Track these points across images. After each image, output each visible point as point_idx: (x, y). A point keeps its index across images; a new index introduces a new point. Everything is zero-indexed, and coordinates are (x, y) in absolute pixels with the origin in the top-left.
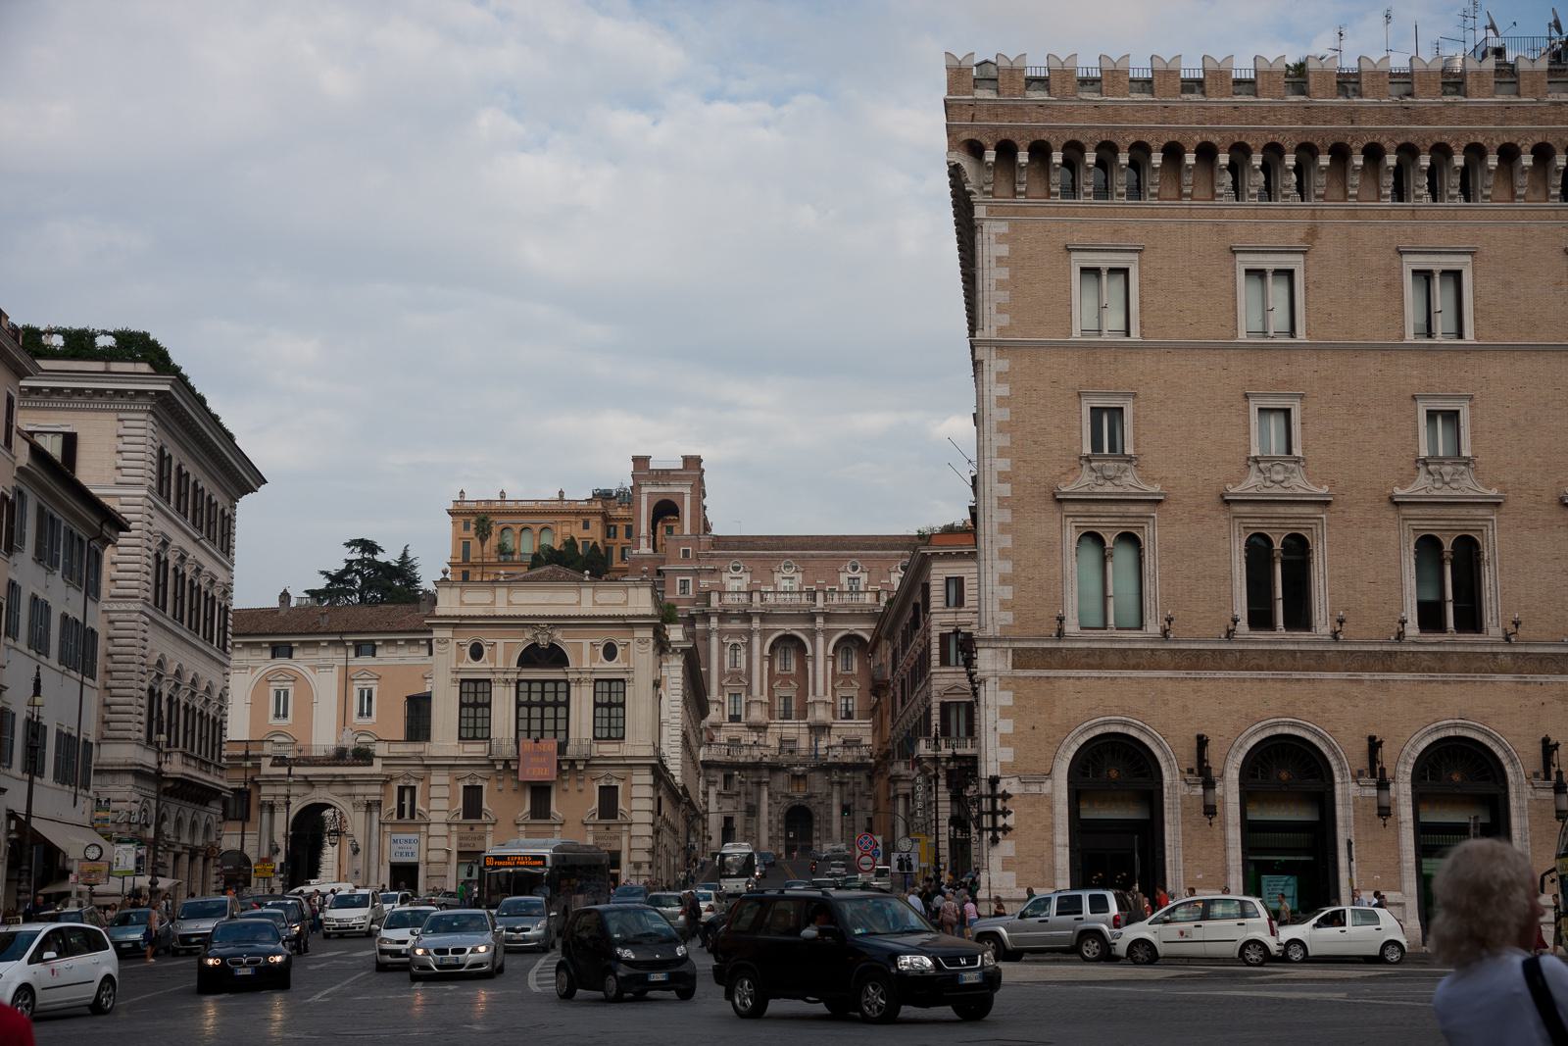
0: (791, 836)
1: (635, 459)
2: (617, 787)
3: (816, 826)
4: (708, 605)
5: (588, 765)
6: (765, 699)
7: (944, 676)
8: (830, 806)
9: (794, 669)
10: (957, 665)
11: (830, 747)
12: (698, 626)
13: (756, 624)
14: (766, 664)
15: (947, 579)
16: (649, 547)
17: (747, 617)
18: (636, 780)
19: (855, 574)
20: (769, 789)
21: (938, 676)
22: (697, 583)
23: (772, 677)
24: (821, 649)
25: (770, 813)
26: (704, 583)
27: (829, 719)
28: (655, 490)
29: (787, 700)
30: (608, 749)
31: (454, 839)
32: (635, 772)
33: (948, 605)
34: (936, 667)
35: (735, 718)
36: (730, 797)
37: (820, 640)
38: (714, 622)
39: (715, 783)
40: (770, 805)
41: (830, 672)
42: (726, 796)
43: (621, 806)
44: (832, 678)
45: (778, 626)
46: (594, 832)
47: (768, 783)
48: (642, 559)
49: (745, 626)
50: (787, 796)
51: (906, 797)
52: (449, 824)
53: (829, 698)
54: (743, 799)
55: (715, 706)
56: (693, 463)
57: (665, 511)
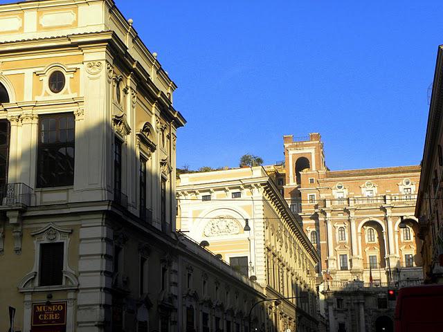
2: (63, 243)
4: (325, 207)
16: (294, 182)
19: (408, 186)
20: (364, 307)
23: (364, 245)
25: (366, 321)
26: (323, 196)
29: (372, 258)
30: (54, 196)
36: (342, 312)
40: (366, 317)
42: (339, 312)
43: (66, 267)
44: (399, 245)
47: (364, 303)
50: (376, 311)
54: (349, 313)
55: (332, 261)
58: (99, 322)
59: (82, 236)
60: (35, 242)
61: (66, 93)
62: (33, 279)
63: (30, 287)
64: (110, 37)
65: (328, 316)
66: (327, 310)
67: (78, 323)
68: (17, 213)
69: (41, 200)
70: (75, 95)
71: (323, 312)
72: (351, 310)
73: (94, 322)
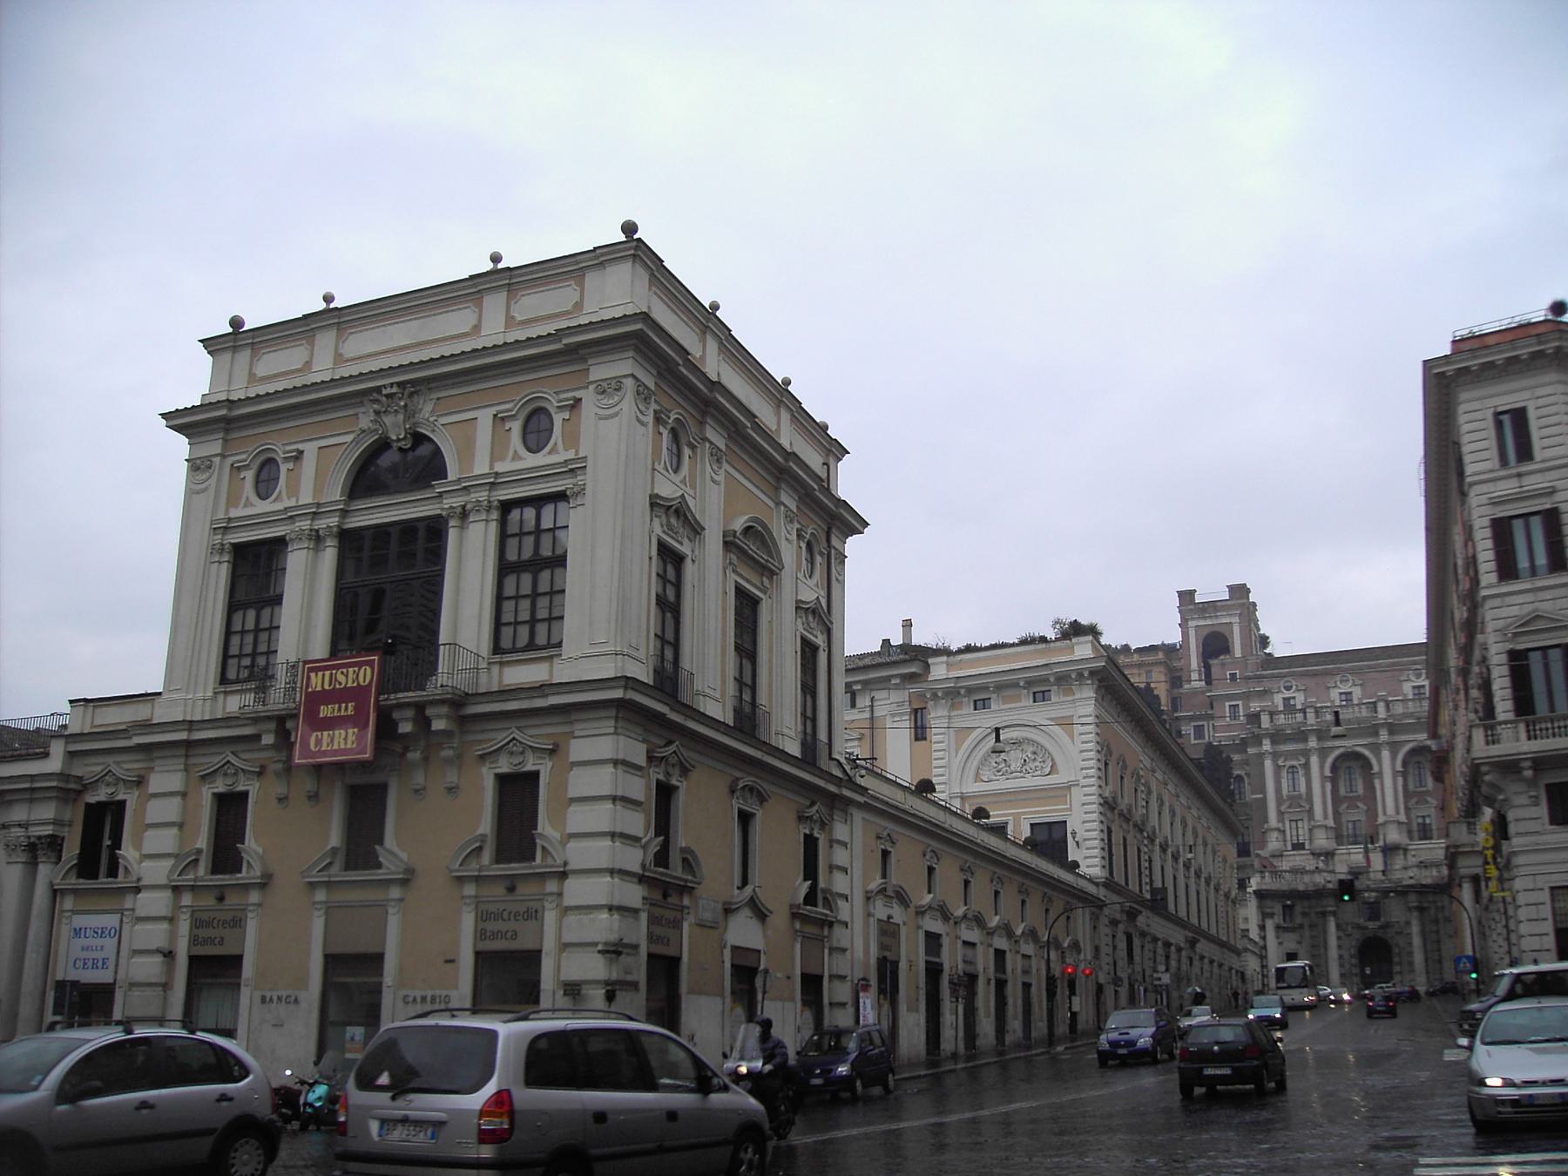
0: (1368, 971)
1: (1180, 594)
2: (535, 776)
3: (1396, 959)
5: (465, 722)
6: (1331, 823)
7: (1509, 600)
8: (1409, 935)
9: (1360, 790)
10: (1533, 571)
11: (1405, 872)
12: (1251, 751)
13: (1313, 743)
14: (1329, 786)
15: (1497, 414)
17: (1301, 736)
18: (579, 749)
20: (1337, 919)
21: (1496, 602)
22: (1246, 707)
23: (1337, 800)
24: (1386, 766)
25: (1340, 947)
26: (1255, 706)
27: (1404, 840)
28: (1202, 623)
31: (184, 926)
32: (579, 729)
33: (1504, 461)
34: (1489, 586)
35: (1298, 846)
36: (1293, 930)
37: (1386, 754)
38: (1267, 746)
39: (1272, 915)
40: (1339, 938)
41: (1400, 788)
42: (1286, 929)
43: (544, 826)
45: (1337, 743)
46: (478, 901)
48: (1195, 692)
49: (1300, 746)
50: (1358, 927)
51: (1475, 880)
52: (176, 889)
53: (1402, 818)
54: (1307, 933)
56: (1240, 591)
57: (1215, 645)
58: (606, 944)
59: (574, 756)
60: (484, 770)
61: (553, 451)
62: (480, 848)
63: (472, 869)
64: (639, 326)
65: (1264, 938)
66: (1262, 928)
67: (567, 946)
68: (444, 710)
69: (500, 681)
70: (571, 455)
71: (1254, 934)
72: (1311, 926)
73: (596, 944)
